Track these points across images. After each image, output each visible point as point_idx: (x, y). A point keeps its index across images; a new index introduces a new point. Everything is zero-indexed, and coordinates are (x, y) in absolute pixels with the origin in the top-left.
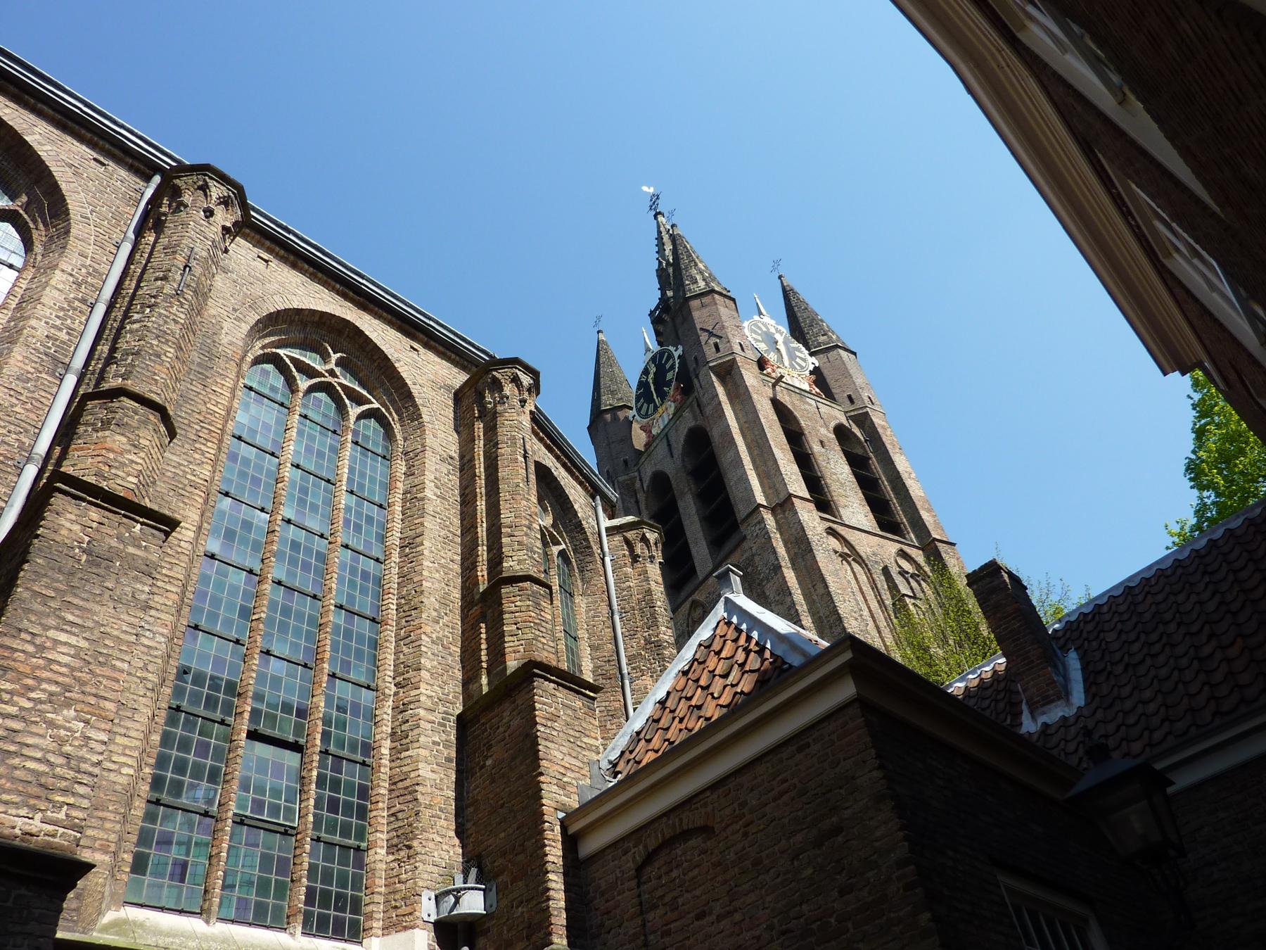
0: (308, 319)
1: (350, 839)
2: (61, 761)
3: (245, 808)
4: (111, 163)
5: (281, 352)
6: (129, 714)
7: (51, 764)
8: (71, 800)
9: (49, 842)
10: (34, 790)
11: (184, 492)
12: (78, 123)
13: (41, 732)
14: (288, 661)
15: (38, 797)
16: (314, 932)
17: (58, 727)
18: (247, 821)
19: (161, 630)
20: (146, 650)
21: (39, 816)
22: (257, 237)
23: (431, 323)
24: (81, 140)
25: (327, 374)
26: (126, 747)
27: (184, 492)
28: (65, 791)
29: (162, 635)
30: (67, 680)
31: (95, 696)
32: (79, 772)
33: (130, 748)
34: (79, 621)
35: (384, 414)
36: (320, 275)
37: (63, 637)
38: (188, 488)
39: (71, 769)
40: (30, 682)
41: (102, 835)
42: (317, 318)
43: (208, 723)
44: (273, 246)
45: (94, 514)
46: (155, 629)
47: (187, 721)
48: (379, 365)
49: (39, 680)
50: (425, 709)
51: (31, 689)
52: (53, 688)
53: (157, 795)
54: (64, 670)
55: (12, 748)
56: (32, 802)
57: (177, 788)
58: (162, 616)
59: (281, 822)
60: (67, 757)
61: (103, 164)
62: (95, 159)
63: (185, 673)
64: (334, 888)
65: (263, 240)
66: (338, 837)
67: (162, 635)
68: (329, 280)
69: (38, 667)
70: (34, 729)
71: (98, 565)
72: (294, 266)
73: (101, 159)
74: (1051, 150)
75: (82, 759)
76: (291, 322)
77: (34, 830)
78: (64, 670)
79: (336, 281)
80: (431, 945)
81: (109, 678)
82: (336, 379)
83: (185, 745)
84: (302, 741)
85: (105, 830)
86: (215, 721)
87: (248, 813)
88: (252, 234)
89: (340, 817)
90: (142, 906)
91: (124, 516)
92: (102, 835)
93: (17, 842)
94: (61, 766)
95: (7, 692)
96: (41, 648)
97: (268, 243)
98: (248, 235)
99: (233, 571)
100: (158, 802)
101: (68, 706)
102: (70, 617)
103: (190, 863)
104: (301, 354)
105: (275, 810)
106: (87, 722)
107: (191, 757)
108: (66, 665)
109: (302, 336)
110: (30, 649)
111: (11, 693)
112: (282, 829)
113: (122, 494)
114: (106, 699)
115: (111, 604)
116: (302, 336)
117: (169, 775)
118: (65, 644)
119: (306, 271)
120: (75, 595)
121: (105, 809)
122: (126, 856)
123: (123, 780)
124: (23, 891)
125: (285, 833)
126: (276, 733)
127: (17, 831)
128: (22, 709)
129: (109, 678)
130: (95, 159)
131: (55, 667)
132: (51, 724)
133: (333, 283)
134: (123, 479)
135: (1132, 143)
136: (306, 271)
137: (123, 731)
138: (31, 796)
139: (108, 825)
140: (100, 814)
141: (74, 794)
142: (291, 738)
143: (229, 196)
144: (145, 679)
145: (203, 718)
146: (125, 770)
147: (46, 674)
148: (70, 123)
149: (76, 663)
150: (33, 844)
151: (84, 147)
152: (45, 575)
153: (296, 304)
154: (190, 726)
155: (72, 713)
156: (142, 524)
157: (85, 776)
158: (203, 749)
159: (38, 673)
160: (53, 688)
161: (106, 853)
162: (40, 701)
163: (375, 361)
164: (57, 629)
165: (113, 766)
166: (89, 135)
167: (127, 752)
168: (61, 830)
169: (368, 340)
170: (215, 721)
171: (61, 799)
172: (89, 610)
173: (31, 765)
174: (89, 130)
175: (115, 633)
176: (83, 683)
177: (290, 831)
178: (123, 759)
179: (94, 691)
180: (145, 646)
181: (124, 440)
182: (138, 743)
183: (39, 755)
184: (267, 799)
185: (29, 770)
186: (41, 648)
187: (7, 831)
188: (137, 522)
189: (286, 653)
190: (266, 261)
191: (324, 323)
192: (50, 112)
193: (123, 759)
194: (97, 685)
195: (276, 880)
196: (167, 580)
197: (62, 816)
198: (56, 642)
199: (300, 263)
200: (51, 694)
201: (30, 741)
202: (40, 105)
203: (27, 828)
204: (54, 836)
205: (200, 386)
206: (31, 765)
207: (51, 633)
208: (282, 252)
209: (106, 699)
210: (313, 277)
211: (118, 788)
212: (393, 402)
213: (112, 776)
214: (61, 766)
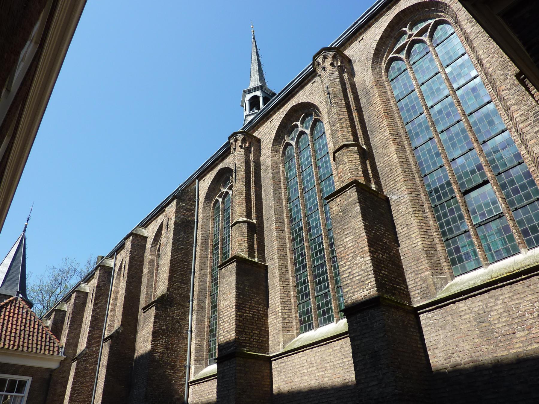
0: (387, 34)
1: (532, 198)
2: (363, 272)
3: (485, 216)
4: (315, 78)
5: (391, 56)
6: (411, 226)
7: (361, 275)
8: (370, 281)
9: (370, 295)
10: (361, 284)
11: (386, 145)
12: (302, 82)
13: (355, 268)
14: (463, 155)
15: (363, 285)
16: (536, 245)
17: (358, 264)
18: (481, 224)
19: (404, 194)
20: (404, 203)
21: (365, 290)
22: (354, 37)
23: (359, 22)
24: (307, 84)
25: (409, 40)
26: (416, 236)
27: (386, 145)
28: (367, 279)
29: (406, 194)
30: (354, 250)
31: (362, 248)
32: (368, 272)
33: (417, 236)
34: (348, 232)
35: (438, 20)
36: (377, 16)
37: (347, 239)
38: (387, 142)
39: (366, 272)
40: (347, 257)
41: (424, 267)
42: (389, 29)
43: (448, 202)
44: (359, 32)
45: (338, 200)
46: (403, 195)
47: (441, 207)
48: (421, 8)
49: (348, 255)
50: (522, 122)
51: (348, 259)
52: (352, 254)
53: (445, 238)
54: (352, 248)
55: (352, 277)
56: (362, 287)
57: (451, 230)
58: (403, 189)
59: (495, 214)
60: (364, 270)
61: (315, 82)
62: (313, 83)
63: (431, 193)
64: (527, 226)
65: (356, 36)
66: (525, 202)
67: (406, 194)
68: (381, 13)
69: (347, 252)
70: (354, 268)
71: (345, 213)
72: (369, 27)
73: (313, 81)
74: (19, 149)
75: (367, 268)
76: (384, 43)
77: (365, 294)
78: (352, 248)
79: (383, 9)
80: (206, 364)
81: (362, 241)
82: (413, 36)
83: (445, 215)
84: (486, 179)
85: (424, 265)
86: (450, 200)
87: (480, 221)
88: (352, 39)
89: (521, 193)
90: (461, 275)
91: (344, 192)
92: (424, 267)
93: (364, 300)
94: (363, 273)
95: (344, 264)
96: (345, 246)
97: (357, 34)
98: (352, 41)
99: (425, 145)
100: (447, 240)
101: (357, 256)
102: (346, 233)
103: (463, 255)
104: (399, 45)
105: (490, 211)
106: (363, 257)
107: (449, 217)
108: (352, 246)
109: (393, 39)
110: (343, 249)
111: (345, 263)
112: (498, 217)
113: (349, 182)
114: (364, 247)
115: (353, 220)
116: (393, 39)
117: (446, 228)
118: (349, 240)
119: (373, 22)
120: (345, 226)
121: (421, 258)
122: (444, 264)
123: (420, 247)
124: (371, 311)
125: (500, 217)
126: (474, 184)
127: (362, 297)
128: (349, 265)
129: (362, 241)
130: (313, 83)
131: (350, 249)
132: (356, 264)
133: (382, 12)
134: (347, 177)
135: (8, 114)
136: (373, 22)
137: (412, 233)
138: (361, 286)
139: (424, 263)
140: (420, 261)
141: (370, 279)
142: (481, 181)
143: (324, 55)
144: (409, 212)
145: (445, 202)
146: (419, 244)
147: (349, 252)
148: (302, 85)
149: (354, 243)
150: (367, 298)
151: (300, 92)
152: (337, 227)
153: (378, 38)
154: (443, 208)
155: (359, 257)
156: (348, 190)
157: (370, 272)
158: (452, 212)
159: (347, 253)
160: (352, 254)
161: (428, 271)
162: (351, 260)
163: (418, 9)
164: (346, 238)
165: (415, 245)
166: (307, 81)
167: (417, 238)
168: (371, 290)
169: (408, 8)
170: (450, 200)
171: (367, 282)
172: (349, 227)
173: (357, 278)
174: (308, 77)
175: (357, 227)
176: (357, 248)
177: (501, 215)
178: (417, 241)
179: (360, 248)
180: (403, 202)
181: (342, 166)
182: (418, 233)
183: (358, 274)
184: (485, 210)
185: (358, 279)
186: (345, 246)
187: (360, 298)
188: (347, 191)
189: (459, 152)
190: (362, 39)
191: (393, 26)
192: (298, 88)
193: (417, 241)
194: (361, 246)
195: (506, 236)
196: (397, 177)
197: (370, 286)
198: (347, 242)
199: (369, 24)
200: (352, 256)
201: (354, 272)
202: (295, 91)
203: (364, 295)
204: (370, 293)
205: (371, 107)
206: (357, 278)
207: (345, 241)
208: (363, 30)
209: (364, 247)
210: (377, 20)
211: (420, 250)
212: (438, 11)
213: (417, 248)
214: (363, 273)
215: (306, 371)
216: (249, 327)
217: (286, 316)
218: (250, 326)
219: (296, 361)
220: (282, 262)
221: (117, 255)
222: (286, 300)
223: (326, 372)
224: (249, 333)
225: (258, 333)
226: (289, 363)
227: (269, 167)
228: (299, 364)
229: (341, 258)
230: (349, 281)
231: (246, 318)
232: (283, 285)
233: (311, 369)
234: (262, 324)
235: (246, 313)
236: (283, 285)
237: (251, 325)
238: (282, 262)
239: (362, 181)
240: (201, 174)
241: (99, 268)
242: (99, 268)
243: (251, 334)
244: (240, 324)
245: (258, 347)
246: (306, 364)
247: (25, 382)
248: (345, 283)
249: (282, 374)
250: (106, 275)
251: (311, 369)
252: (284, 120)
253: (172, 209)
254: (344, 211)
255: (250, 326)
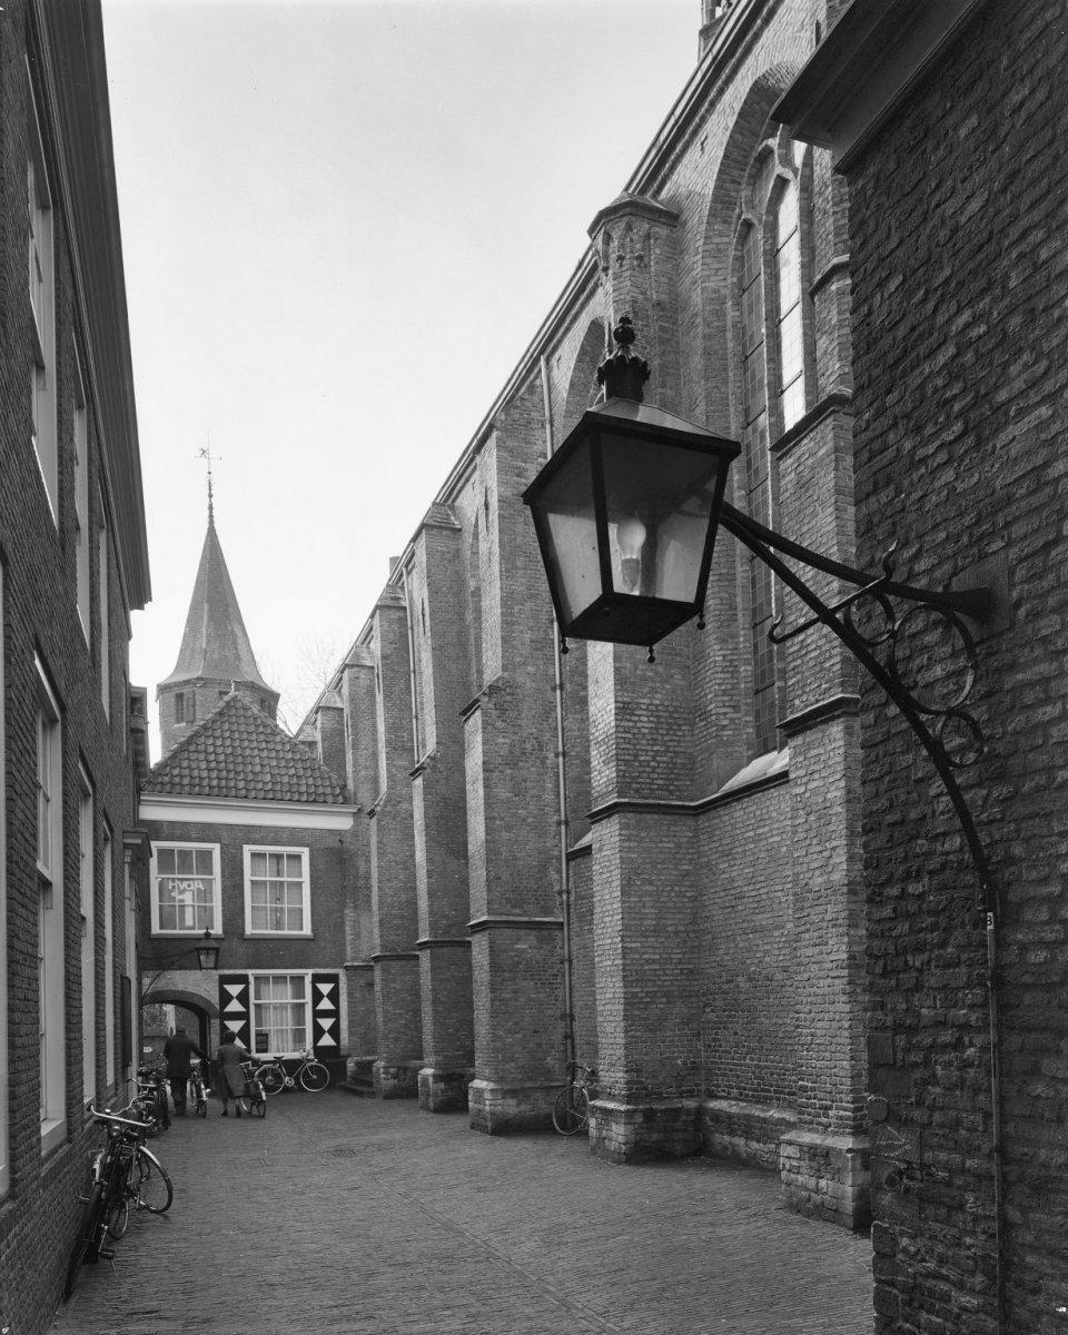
2: (824, 640)
215: (752, 834)
216: (647, 751)
217: (726, 722)
218: (649, 748)
219: (738, 814)
220: (723, 595)
221: (548, 360)
222: (729, 687)
223: (784, 836)
224: (648, 761)
225: (669, 760)
226: (726, 818)
227: (696, 314)
228: (743, 822)
229: (790, 608)
230: (799, 662)
231: (640, 732)
232: (722, 652)
233: (760, 831)
234: (679, 741)
235: (641, 721)
236: (722, 652)
237: (652, 746)
238: (723, 595)
239: (873, 378)
240: (547, 344)
241: (43, 1153)
242: (43, 1153)
243: (652, 764)
244: (628, 746)
245: (668, 790)
246: (753, 821)
247: (210, 853)
248: (792, 665)
249: (715, 838)
250: (395, 626)
251: (760, 831)
252: (737, 136)
253: (490, 458)
254: (803, 485)
255: (649, 748)
